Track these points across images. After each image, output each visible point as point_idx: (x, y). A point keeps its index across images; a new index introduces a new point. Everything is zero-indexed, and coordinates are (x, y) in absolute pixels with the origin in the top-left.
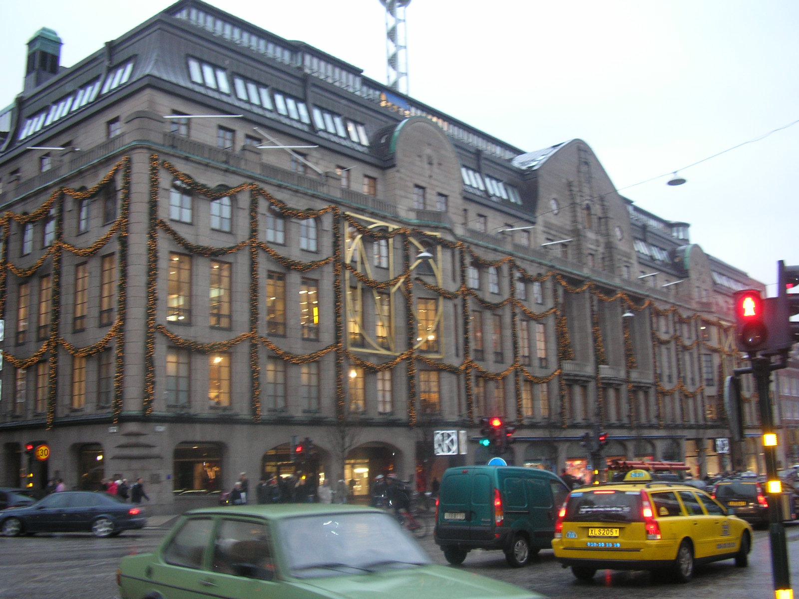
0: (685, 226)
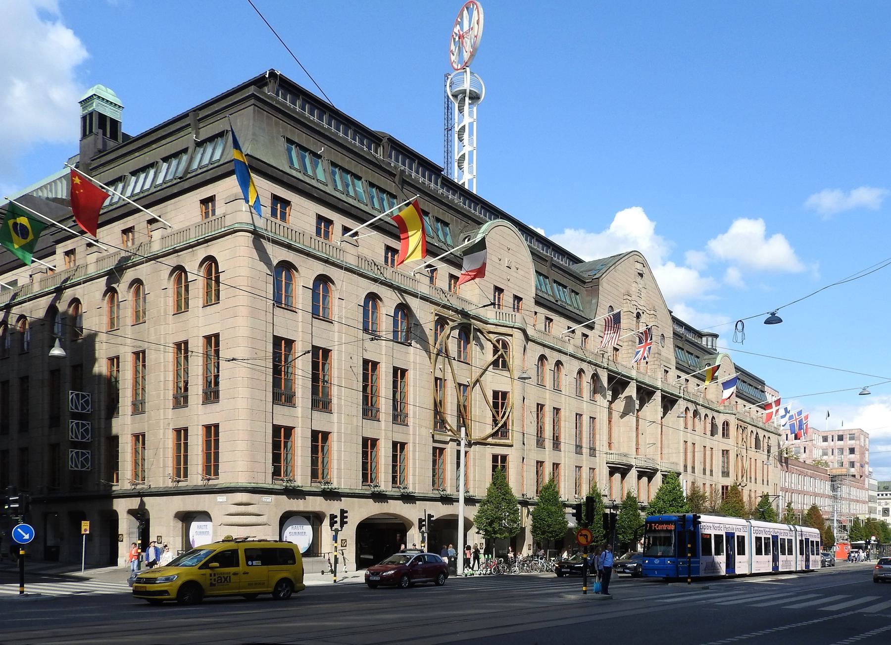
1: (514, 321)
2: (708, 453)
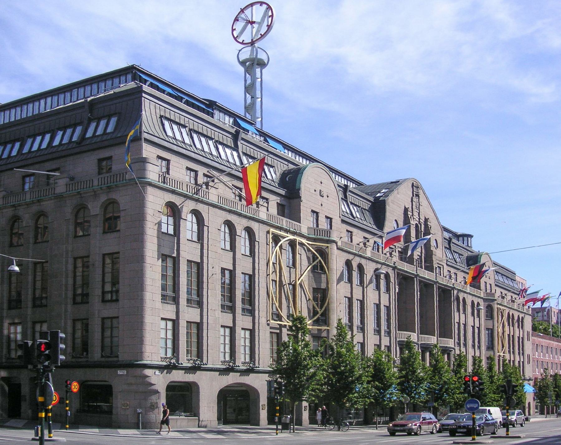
0: (471, 236)
1: (329, 236)
2: (476, 331)
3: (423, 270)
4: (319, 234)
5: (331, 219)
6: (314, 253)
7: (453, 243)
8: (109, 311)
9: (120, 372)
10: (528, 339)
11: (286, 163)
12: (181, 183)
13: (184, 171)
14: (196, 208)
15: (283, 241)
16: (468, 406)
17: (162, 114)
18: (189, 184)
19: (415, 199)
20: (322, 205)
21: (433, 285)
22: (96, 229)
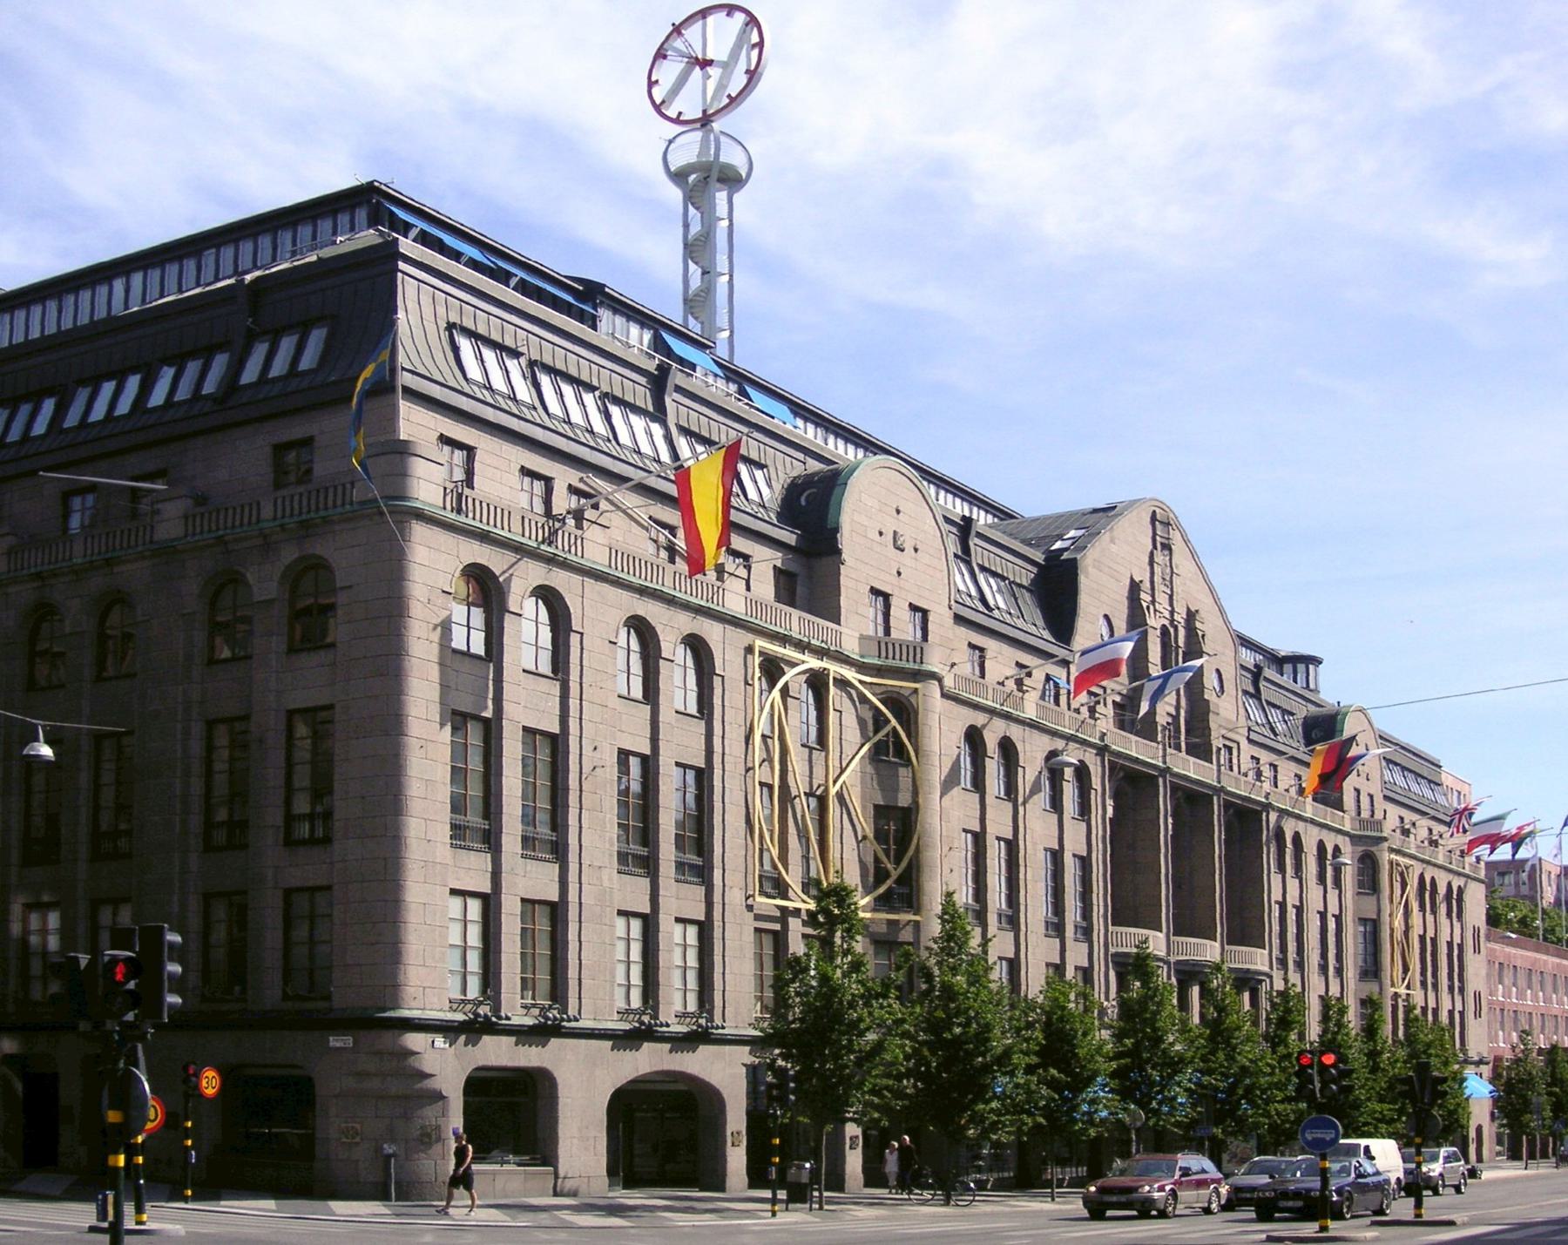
0: (1316, 661)
1: (918, 660)
2: (1332, 925)
3: (1183, 754)
4: (891, 655)
5: (925, 612)
6: (877, 709)
7: (1267, 680)
8: (305, 870)
9: (335, 1042)
10: (1477, 950)
11: (801, 456)
12: (506, 513)
13: (515, 478)
14: (547, 583)
15: (790, 674)
16: (1309, 1137)
17: (454, 318)
18: (529, 515)
19: (1160, 557)
20: (899, 574)
21: (1210, 798)
22: (270, 643)
